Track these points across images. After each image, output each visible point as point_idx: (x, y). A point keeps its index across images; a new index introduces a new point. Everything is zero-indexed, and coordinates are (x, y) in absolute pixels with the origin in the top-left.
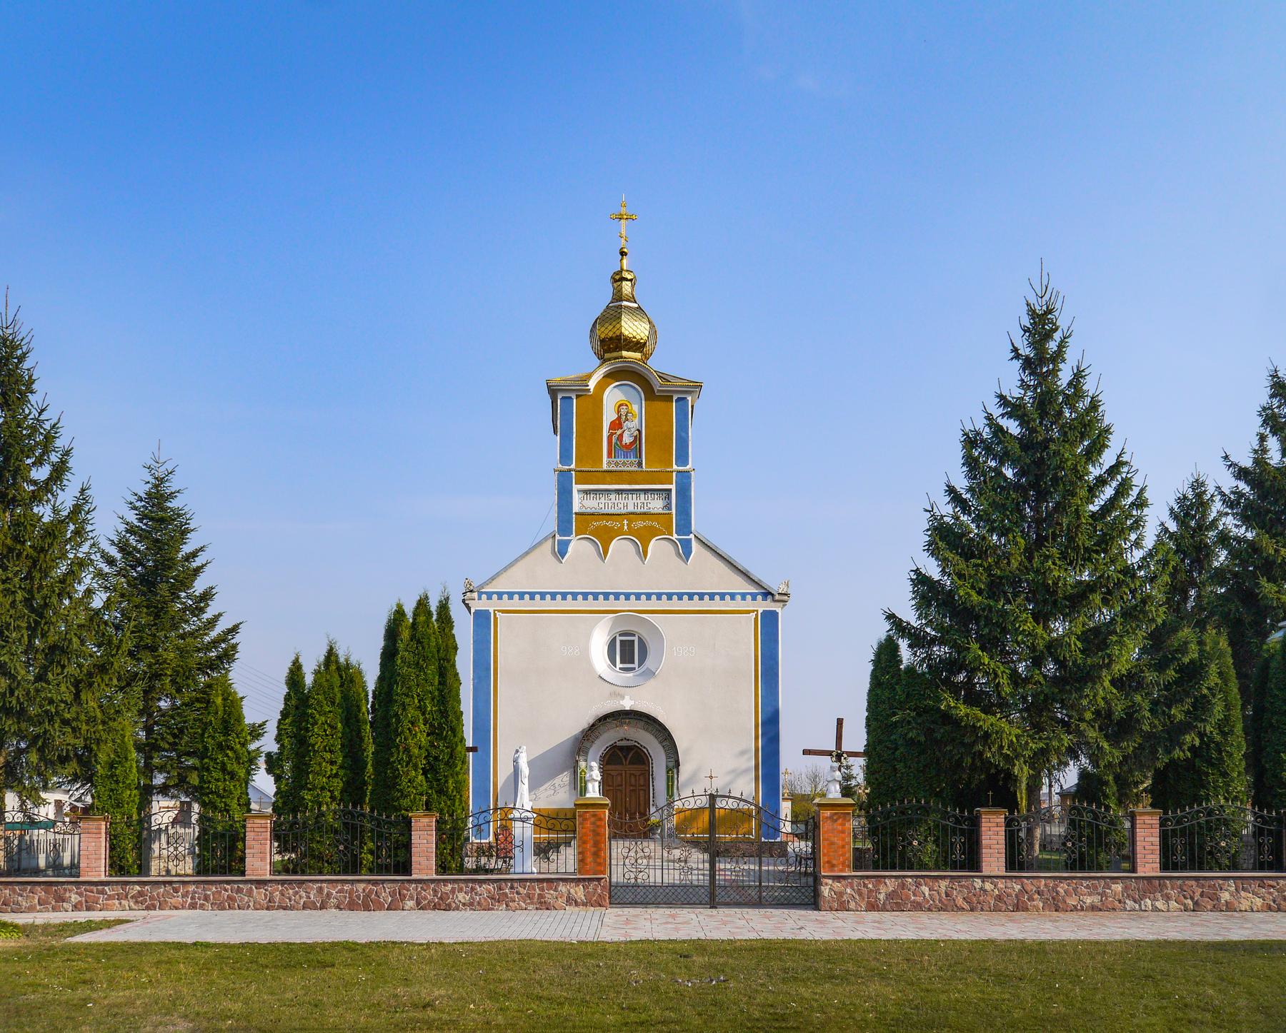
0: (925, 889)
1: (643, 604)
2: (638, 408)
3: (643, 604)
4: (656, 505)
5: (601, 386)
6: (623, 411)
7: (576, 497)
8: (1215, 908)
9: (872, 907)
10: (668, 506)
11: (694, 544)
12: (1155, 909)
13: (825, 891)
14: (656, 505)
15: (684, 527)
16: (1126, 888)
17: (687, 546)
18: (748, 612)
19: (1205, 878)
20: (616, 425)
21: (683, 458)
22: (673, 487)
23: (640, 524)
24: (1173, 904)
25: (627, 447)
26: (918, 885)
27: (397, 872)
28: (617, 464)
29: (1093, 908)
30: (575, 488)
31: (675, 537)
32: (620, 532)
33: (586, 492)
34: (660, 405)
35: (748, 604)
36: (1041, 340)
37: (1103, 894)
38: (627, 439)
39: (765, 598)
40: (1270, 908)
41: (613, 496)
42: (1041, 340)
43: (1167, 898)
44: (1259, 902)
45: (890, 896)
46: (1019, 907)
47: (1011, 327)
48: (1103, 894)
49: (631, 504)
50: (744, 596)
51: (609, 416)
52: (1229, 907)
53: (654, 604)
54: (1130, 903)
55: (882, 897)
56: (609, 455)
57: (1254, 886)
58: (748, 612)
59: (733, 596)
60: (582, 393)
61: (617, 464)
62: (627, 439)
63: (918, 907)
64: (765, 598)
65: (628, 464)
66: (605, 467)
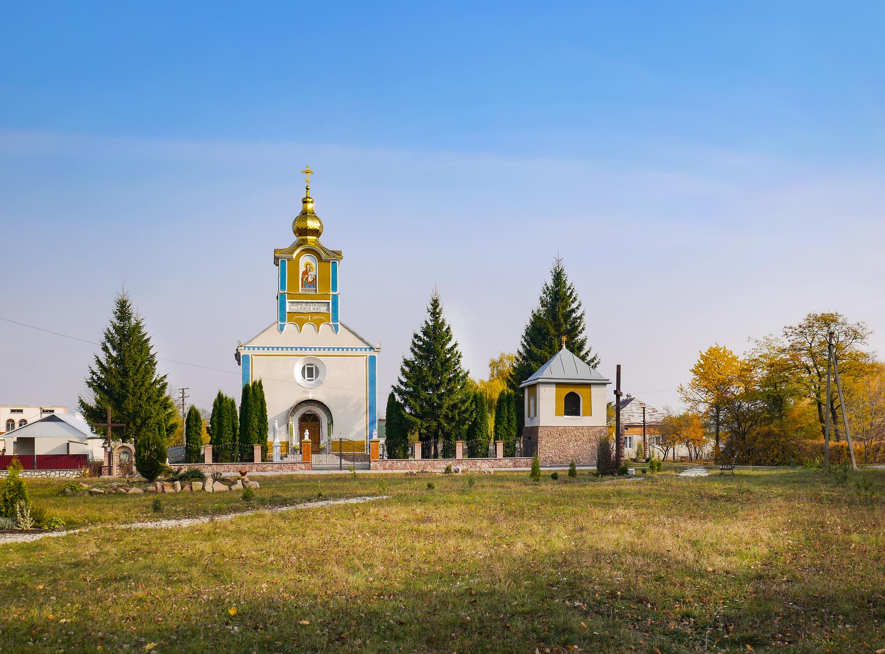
1: (317, 352)
3: (317, 352)
4: (323, 309)
5: (299, 256)
7: (287, 305)
10: (328, 309)
11: (340, 326)
15: (335, 319)
17: (336, 327)
20: (305, 273)
21: (335, 288)
23: (316, 317)
35: (363, 353)
38: (310, 279)
42: (558, 277)
49: (312, 308)
50: (361, 349)
51: (302, 269)
53: (322, 352)
59: (356, 349)
62: (310, 279)
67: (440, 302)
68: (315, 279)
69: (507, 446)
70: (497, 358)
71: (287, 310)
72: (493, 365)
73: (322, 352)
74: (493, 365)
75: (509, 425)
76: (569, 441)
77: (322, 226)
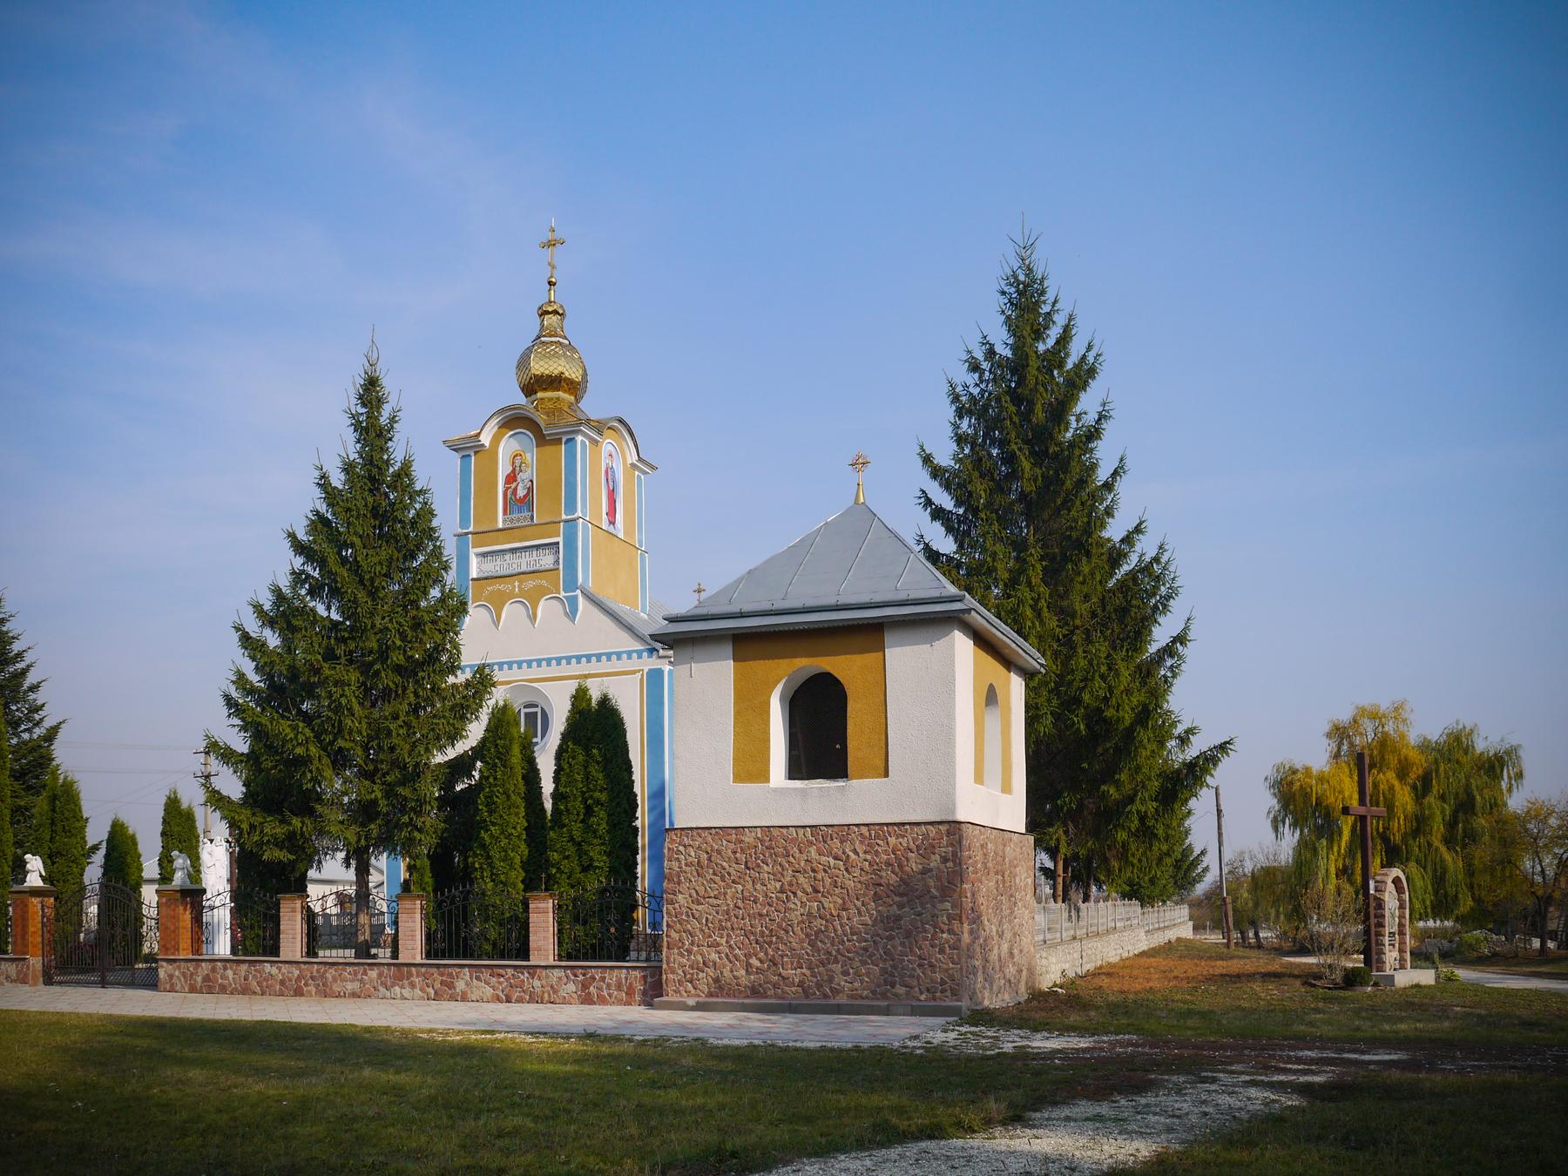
0: (230, 973)
1: (535, 672)
2: (531, 456)
3: (535, 672)
4: (547, 560)
5: (496, 440)
6: (517, 463)
7: (474, 562)
8: (453, 998)
9: (193, 990)
10: (557, 561)
11: (581, 599)
12: (403, 998)
13: (162, 974)
14: (547, 560)
15: (571, 584)
16: (380, 975)
17: (573, 602)
18: (634, 672)
19: (445, 966)
20: (511, 478)
21: (571, 507)
22: (560, 539)
23: (530, 583)
24: (418, 992)
25: (521, 500)
26: (225, 968)
27: (517, 958)
28: (512, 521)
29: (354, 995)
30: (472, 552)
31: (562, 594)
32: (511, 595)
33: (484, 555)
34: (549, 449)
35: (634, 663)
36: (1026, 303)
37: (361, 981)
38: (521, 493)
39: (650, 656)
40: (499, 1000)
41: (507, 557)
42: (1026, 303)
43: (413, 986)
44: (489, 991)
45: (206, 979)
46: (299, 993)
47: (343, 398)
48: (361, 981)
49: (524, 562)
50: (629, 654)
51: (503, 470)
52: (464, 998)
53: (544, 672)
54: (382, 989)
55: (199, 979)
56: (505, 513)
57: (486, 975)
58: (634, 672)
59: (619, 655)
60: (479, 449)
61: (512, 521)
62: (521, 493)
63: (223, 989)
64: (650, 656)
65: (520, 517)
66: (500, 526)
67: (388, 384)
68: (530, 490)
69: (569, 917)
70: (1344, 716)
71: (474, 574)
72: (1339, 733)
73: (544, 672)
74: (1339, 733)
75: (588, 828)
76: (788, 891)
77: (585, 375)
